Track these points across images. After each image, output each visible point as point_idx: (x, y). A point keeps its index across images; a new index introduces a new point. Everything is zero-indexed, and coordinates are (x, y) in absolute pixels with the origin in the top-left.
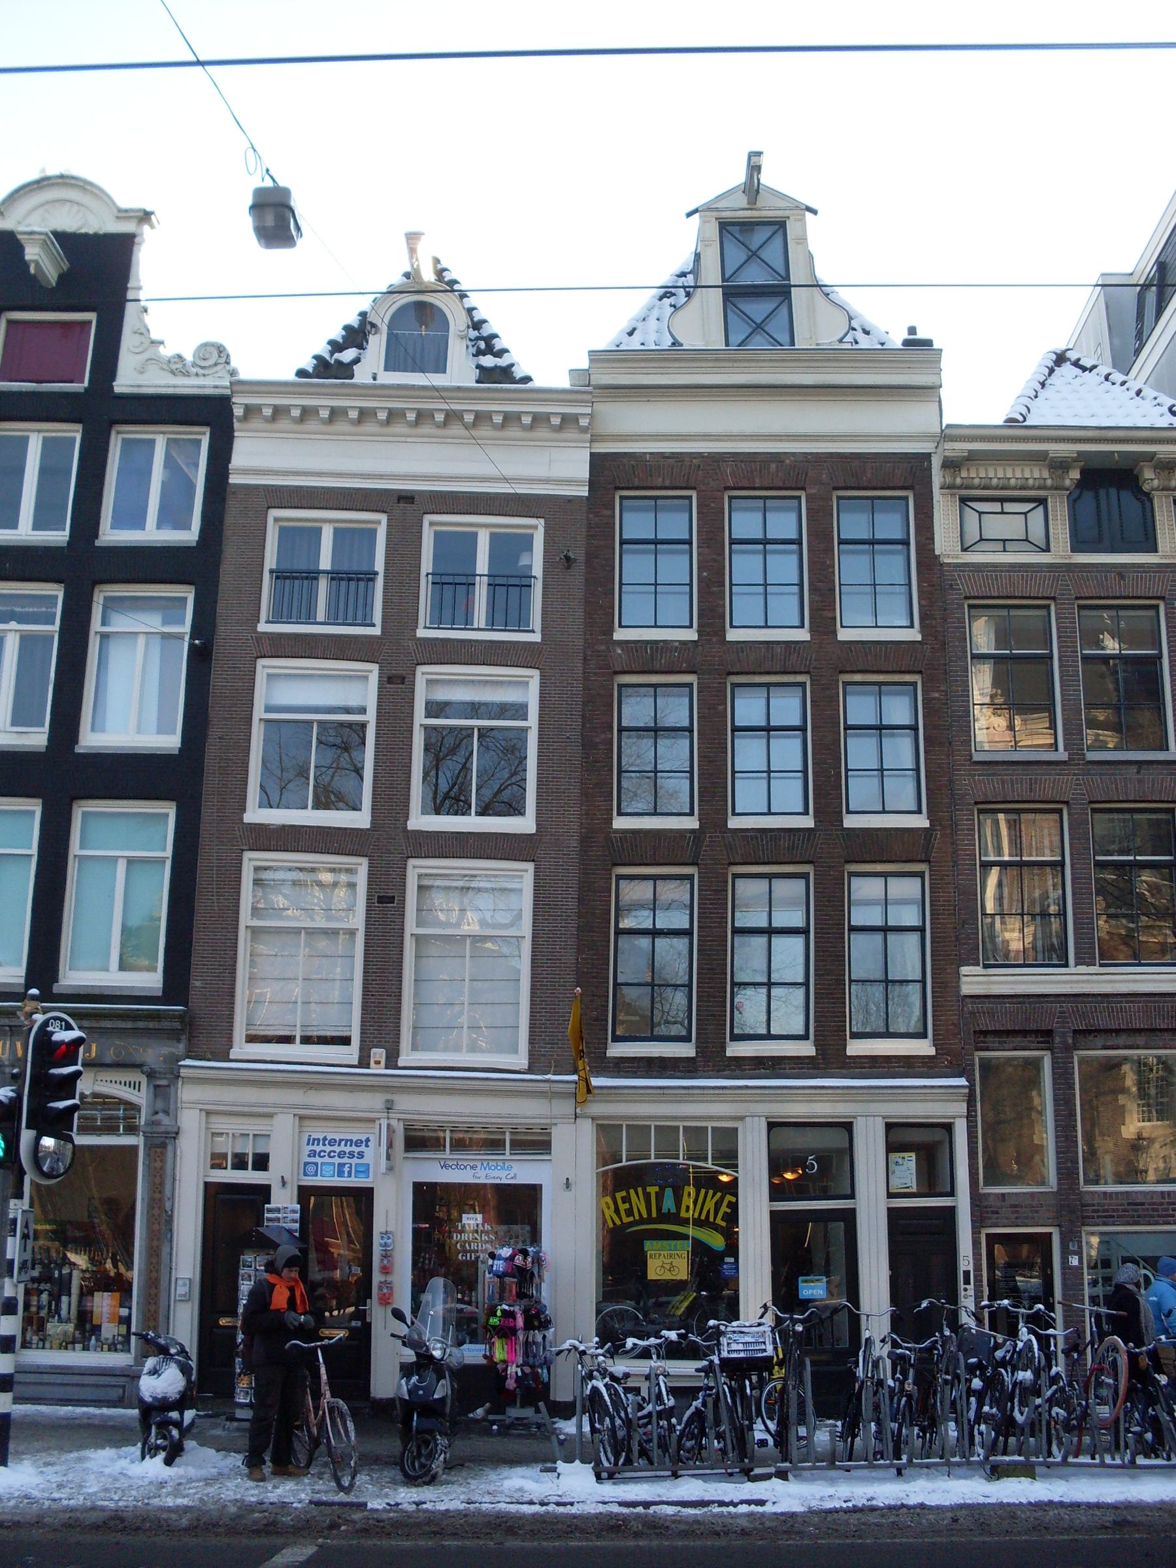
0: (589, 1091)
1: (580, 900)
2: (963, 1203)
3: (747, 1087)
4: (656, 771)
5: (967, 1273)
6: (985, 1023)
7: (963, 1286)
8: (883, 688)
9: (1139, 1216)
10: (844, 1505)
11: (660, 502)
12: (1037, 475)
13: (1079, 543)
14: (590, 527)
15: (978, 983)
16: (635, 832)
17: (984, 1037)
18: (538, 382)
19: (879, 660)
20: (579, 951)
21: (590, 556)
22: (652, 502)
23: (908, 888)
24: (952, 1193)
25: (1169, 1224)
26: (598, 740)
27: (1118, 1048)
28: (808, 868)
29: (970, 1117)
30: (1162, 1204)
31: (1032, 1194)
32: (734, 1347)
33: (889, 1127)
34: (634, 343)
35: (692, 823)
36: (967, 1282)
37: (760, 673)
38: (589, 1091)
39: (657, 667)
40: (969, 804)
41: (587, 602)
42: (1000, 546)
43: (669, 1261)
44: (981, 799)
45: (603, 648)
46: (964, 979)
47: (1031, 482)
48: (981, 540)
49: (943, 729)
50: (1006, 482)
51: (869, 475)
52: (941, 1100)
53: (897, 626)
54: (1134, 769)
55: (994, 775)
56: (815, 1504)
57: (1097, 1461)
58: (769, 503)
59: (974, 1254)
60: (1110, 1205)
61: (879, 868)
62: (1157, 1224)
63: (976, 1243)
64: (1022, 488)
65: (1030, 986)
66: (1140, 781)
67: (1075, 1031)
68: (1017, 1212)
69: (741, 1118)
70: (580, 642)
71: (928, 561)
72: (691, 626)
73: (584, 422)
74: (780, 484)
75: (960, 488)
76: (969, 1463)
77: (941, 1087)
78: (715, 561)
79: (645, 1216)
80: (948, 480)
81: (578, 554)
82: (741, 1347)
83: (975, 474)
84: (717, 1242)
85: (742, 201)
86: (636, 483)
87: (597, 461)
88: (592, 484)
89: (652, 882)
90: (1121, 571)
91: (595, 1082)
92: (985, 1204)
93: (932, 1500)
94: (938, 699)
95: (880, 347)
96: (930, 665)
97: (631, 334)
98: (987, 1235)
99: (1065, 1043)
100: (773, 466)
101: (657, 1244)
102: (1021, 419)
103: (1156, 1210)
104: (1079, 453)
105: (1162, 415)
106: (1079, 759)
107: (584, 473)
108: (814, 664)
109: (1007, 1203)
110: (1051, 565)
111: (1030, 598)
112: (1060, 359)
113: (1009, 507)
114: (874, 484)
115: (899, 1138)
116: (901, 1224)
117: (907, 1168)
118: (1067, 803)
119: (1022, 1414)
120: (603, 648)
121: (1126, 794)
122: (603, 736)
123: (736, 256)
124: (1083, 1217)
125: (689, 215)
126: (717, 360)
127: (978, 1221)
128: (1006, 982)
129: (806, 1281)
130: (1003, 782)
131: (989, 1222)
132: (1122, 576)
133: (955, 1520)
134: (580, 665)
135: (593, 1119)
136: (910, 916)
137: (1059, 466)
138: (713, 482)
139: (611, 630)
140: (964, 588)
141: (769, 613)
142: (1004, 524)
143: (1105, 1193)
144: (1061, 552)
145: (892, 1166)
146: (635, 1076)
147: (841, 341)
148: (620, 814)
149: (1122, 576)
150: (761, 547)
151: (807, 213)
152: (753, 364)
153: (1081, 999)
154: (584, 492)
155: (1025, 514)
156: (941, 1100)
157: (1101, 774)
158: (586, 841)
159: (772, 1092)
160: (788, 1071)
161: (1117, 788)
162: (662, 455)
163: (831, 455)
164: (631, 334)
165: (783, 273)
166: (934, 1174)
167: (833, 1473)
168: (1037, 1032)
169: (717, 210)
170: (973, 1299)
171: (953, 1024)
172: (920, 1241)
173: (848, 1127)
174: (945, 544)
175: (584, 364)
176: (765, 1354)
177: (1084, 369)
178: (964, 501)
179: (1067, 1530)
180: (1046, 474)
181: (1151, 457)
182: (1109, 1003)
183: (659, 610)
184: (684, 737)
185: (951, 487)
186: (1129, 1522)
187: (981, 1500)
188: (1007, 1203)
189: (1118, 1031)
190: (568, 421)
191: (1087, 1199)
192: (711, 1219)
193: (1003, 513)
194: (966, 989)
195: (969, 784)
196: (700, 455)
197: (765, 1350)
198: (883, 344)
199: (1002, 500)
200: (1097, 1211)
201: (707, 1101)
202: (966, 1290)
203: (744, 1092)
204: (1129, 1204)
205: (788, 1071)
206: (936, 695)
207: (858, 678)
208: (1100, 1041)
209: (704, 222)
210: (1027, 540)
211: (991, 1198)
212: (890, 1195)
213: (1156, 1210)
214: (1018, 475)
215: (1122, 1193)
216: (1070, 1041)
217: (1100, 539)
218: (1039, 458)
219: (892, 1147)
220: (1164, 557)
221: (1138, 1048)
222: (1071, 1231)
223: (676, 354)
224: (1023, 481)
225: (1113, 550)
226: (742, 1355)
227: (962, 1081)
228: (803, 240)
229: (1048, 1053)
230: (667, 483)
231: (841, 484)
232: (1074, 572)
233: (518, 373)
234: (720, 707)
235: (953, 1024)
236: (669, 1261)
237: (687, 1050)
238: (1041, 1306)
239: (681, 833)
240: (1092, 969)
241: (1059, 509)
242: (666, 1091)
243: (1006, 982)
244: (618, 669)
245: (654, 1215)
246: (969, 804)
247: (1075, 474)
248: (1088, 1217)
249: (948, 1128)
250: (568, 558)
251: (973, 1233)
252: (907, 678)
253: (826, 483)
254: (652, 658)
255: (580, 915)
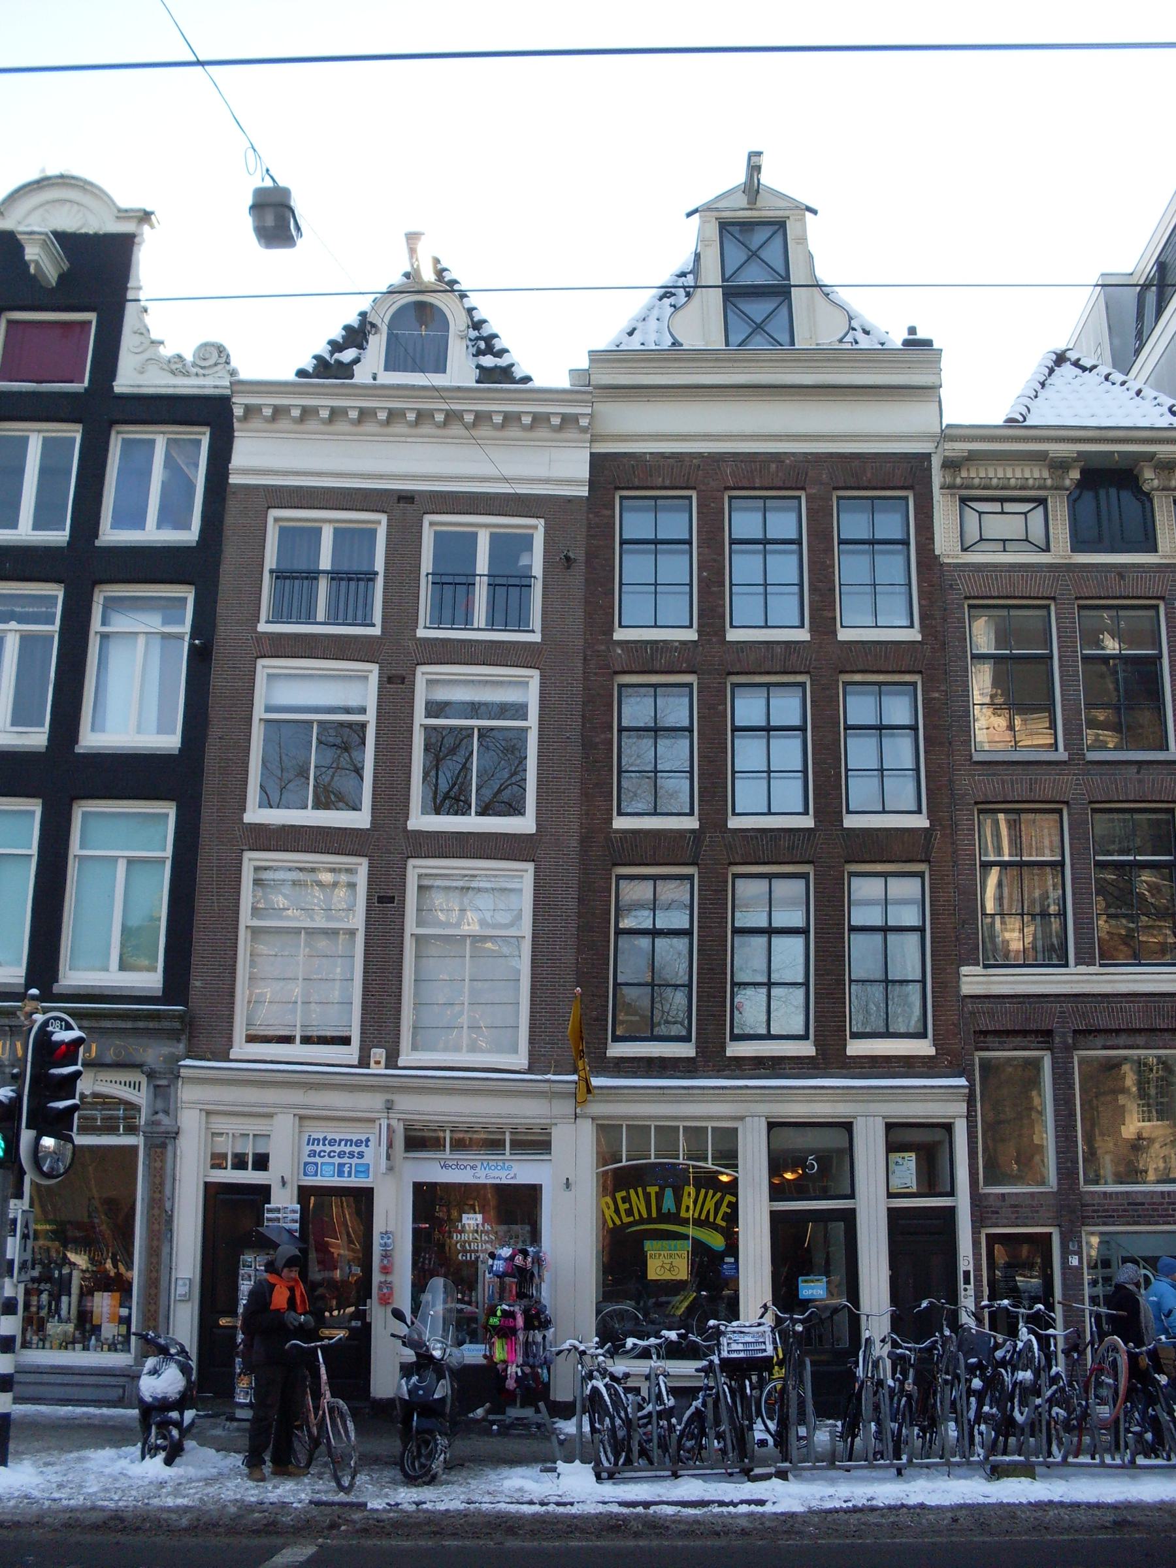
0: (589, 1091)
1: (580, 900)
2: (963, 1203)
3: (747, 1087)
4: (656, 771)
5: (967, 1273)
6: (985, 1023)
7: (963, 1286)
8: (883, 688)
9: (1139, 1216)
10: (844, 1505)
11: (660, 502)
12: (1037, 475)
13: (1079, 543)
14: (590, 527)
15: (978, 983)
16: (635, 832)
17: (984, 1037)
18: (538, 382)
19: (879, 660)
20: (579, 951)
21: (590, 556)
22: (652, 502)
23: (908, 888)
24: (952, 1193)
25: (1169, 1224)
26: (598, 740)
27: (1118, 1048)
28: (808, 868)
29: (970, 1117)
30: (1162, 1204)
31: (1032, 1194)
32: (734, 1347)
33: (889, 1127)
34: (634, 343)
35: (692, 823)
36: (967, 1282)
37: (760, 673)
38: (589, 1091)
39: (657, 667)
40: (969, 804)
41: (587, 602)
42: (1000, 546)
43: (669, 1261)
44: (981, 799)
45: (603, 648)
46: (964, 979)
47: (1031, 482)
48: (981, 540)
49: (943, 729)
50: (1006, 482)
51: (869, 475)
52: (941, 1100)
53: (897, 626)
54: (1134, 769)
55: (994, 775)
56: (815, 1504)
57: (1097, 1461)
58: (769, 503)
59: (974, 1254)
60: (1110, 1205)
61: (879, 868)
62: (1157, 1224)
63: (976, 1243)
64: (1022, 488)
65: (1030, 986)
66: (1140, 781)
67: (1075, 1031)
68: (1017, 1212)
69: (741, 1118)
70: (580, 642)
71: (928, 561)
72: (691, 626)
73: (584, 422)
74: (780, 484)
75: (960, 488)
76: (969, 1463)
77: (941, 1087)
78: (715, 561)
79: (645, 1216)
80: (948, 480)
81: (578, 554)
82: (741, 1347)
83: (975, 474)
84: (717, 1242)
85: (742, 201)
86: (636, 483)
87: (597, 461)
88: (592, 484)
89: (652, 882)
90: (1121, 571)
91: (595, 1082)
92: (985, 1204)
93: (932, 1500)
94: (938, 699)
95: (880, 347)
96: (930, 665)
97: (631, 334)
98: (987, 1235)
99: (1065, 1043)
100: (773, 466)
101: (657, 1244)
102: (1021, 419)
103: (1156, 1210)
104: (1079, 453)
105: (1162, 415)
106: (1079, 759)
107: (584, 473)
108: (814, 664)
109: (1007, 1203)
110: (1051, 565)
111: (1030, 598)
112: (1060, 359)
113: (1009, 507)
114: (874, 484)
115: (899, 1138)
116: (901, 1224)
117: (907, 1168)
118: (1067, 803)
119: (1022, 1414)
120: (603, 648)
121: (1126, 794)
122: (603, 736)
123: (736, 256)
124: (1083, 1217)
125: (689, 215)
126: (717, 360)
127: (978, 1221)
128: (1006, 982)
129: (806, 1281)
130: (1003, 782)
131: (989, 1222)
132: (1122, 576)
133: (955, 1520)
134: (580, 665)
135: (593, 1119)
136: (910, 916)
137: (1059, 466)
138: (713, 482)
139: (611, 630)
140: (964, 588)
141: (769, 613)
142: (1004, 524)
143: (1105, 1193)
144: (1061, 552)
145: (892, 1166)
146: (635, 1076)
147: (841, 341)
148: (620, 814)
149: (1122, 576)
150: (761, 547)
151: (807, 213)
152: (753, 364)
153: (1081, 999)
154: (584, 492)
155: (1025, 514)
156: (941, 1100)
157: (1101, 774)
158: (586, 841)
159: (772, 1092)
160: (788, 1071)
161: (1117, 788)
162: (662, 455)
163: (831, 455)
164: (631, 334)
165: (783, 273)
166: (934, 1174)
167: (833, 1473)
168: (1037, 1032)
169: (717, 210)
170: (973, 1299)
171: (953, 1024)
172: (920, 1241)
173: (848, 1127)
174: (945, 544)
175: (584, 364)
176: (765, 1354)
177: (1084, 369)
178: (964, 501)
179: (1067, 1530)
180: (1046, 474)
181: (1151, 457)
182: (1109, 1003)
183: (659, 610)
184: (684, 737)
185: (951, 487)
186: (1129, 1522)
187: (981, 1500)
188: (1007, 1203)
189: (1118, 1031)
190: (568, 421)
191: (1087, 1199)
192: (711, 1219)
193: (1003, 513)
194: (966, 989)
195: (969, 784)
196: (700, 455)
197: (765, 1350)
198: (883, 344)
199: (1002, 500)
200: (1097, 1211)
201: (707, 1101)
202: (966, 1290)
203: (744, 1092)
204: (1129, 1204)
205: (788, 1071)
206: (936, 695)
207: (858, 678)
208: (1100, 1041)
209: (704, 222)
210: (1027, 540)
211: (991, 1198)
212: (890, 1195)
213: (1156, 1210)
214: (1018, 475)
215: (1122, 1193)
216: (1070, 1041)
217: (1100, 539)
218: (1039, 458)
219: (892, 1147)
220: (1164, 557)
221: (1138, 1048)
222: (1071, 1231)
223: (676, 354)
224: (1023, 481)
225: (1113, 550)
226: (742, 1355)
227: (962, 1081)
228: (803, 240)
229: (1048, 1053)
230: (667, 483)
231: (841, 484)
232: (1074, 572)
233: (518, 373)
234: (720, 707)
235: (953, 1024)
236: (669, 1261)
237: (687, 1050)
238: (1041, 1306)
239: (681, 833)
240: (1092, 969)
241: (1059, 509)
242: (666, 1091)
243: (1006, 982)
244: (618, 669)
245: (654, 1215)
246: (969, 804)
247: (1075, 474)
248: (1088, 1217)
249: (948, 1128)
250: (568, 558)
251: (973, 1233)
252: (907, 678)
253: (826, 483)
254: (652, 658)
255: (580, 915)
